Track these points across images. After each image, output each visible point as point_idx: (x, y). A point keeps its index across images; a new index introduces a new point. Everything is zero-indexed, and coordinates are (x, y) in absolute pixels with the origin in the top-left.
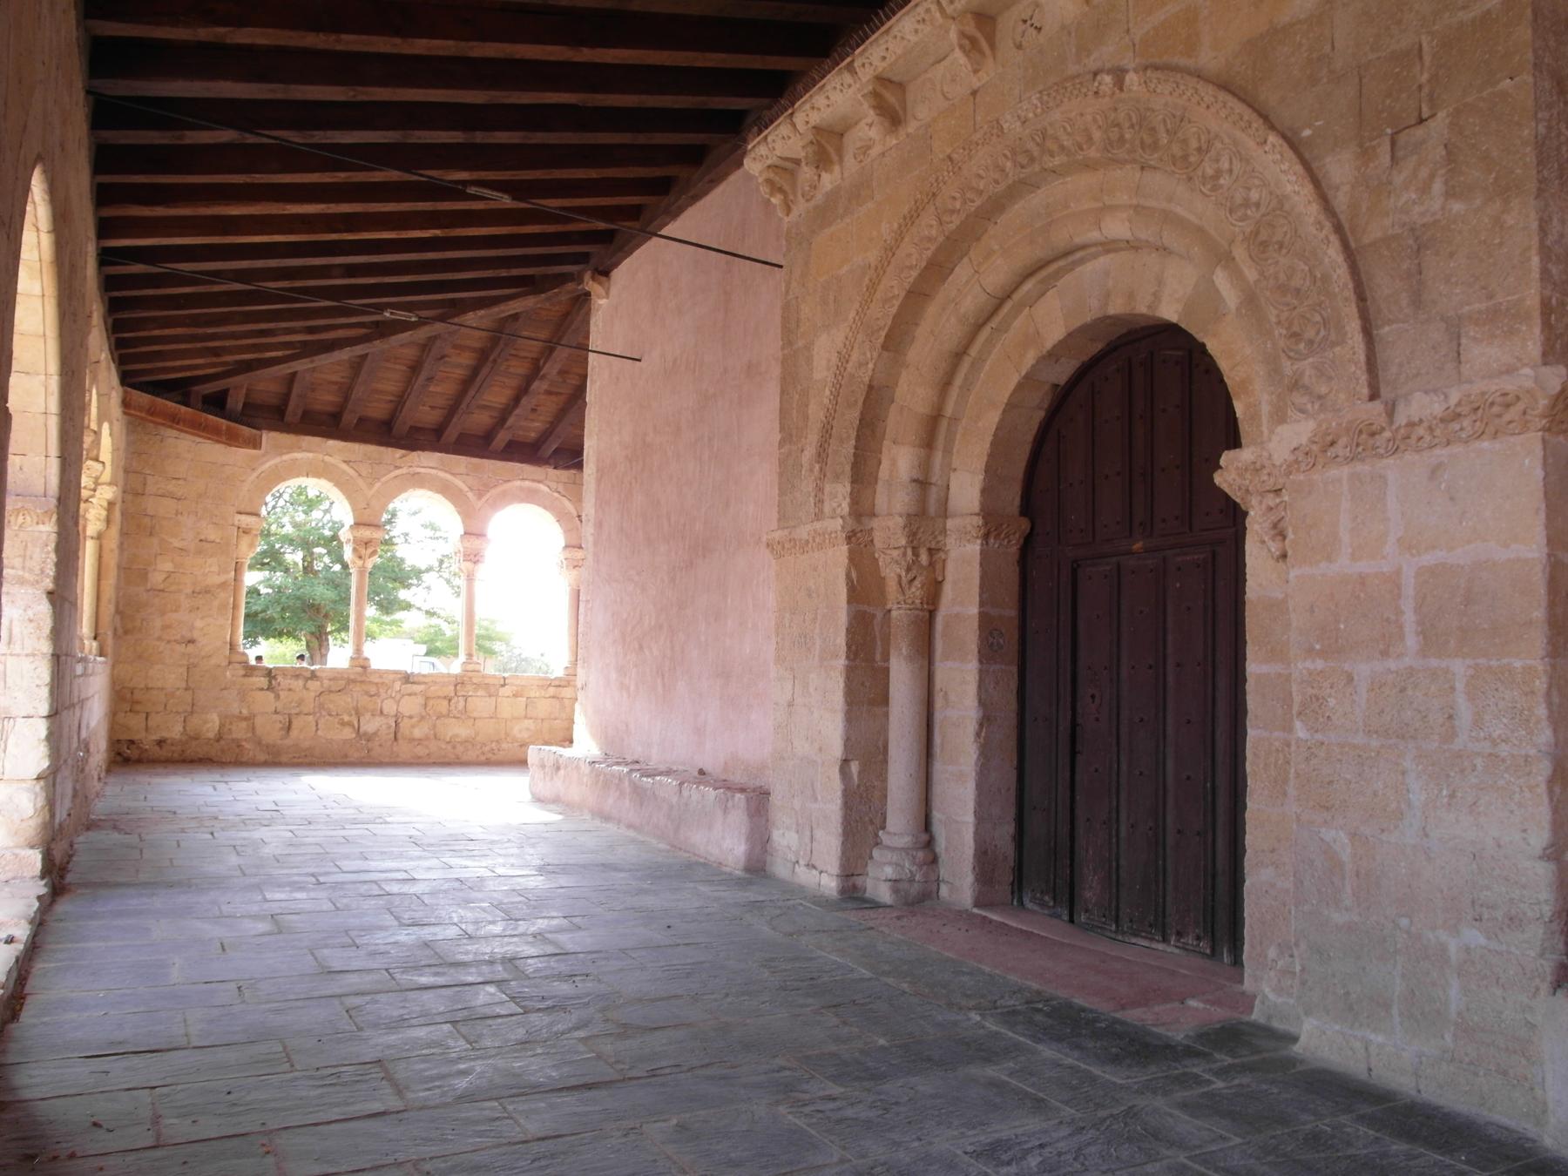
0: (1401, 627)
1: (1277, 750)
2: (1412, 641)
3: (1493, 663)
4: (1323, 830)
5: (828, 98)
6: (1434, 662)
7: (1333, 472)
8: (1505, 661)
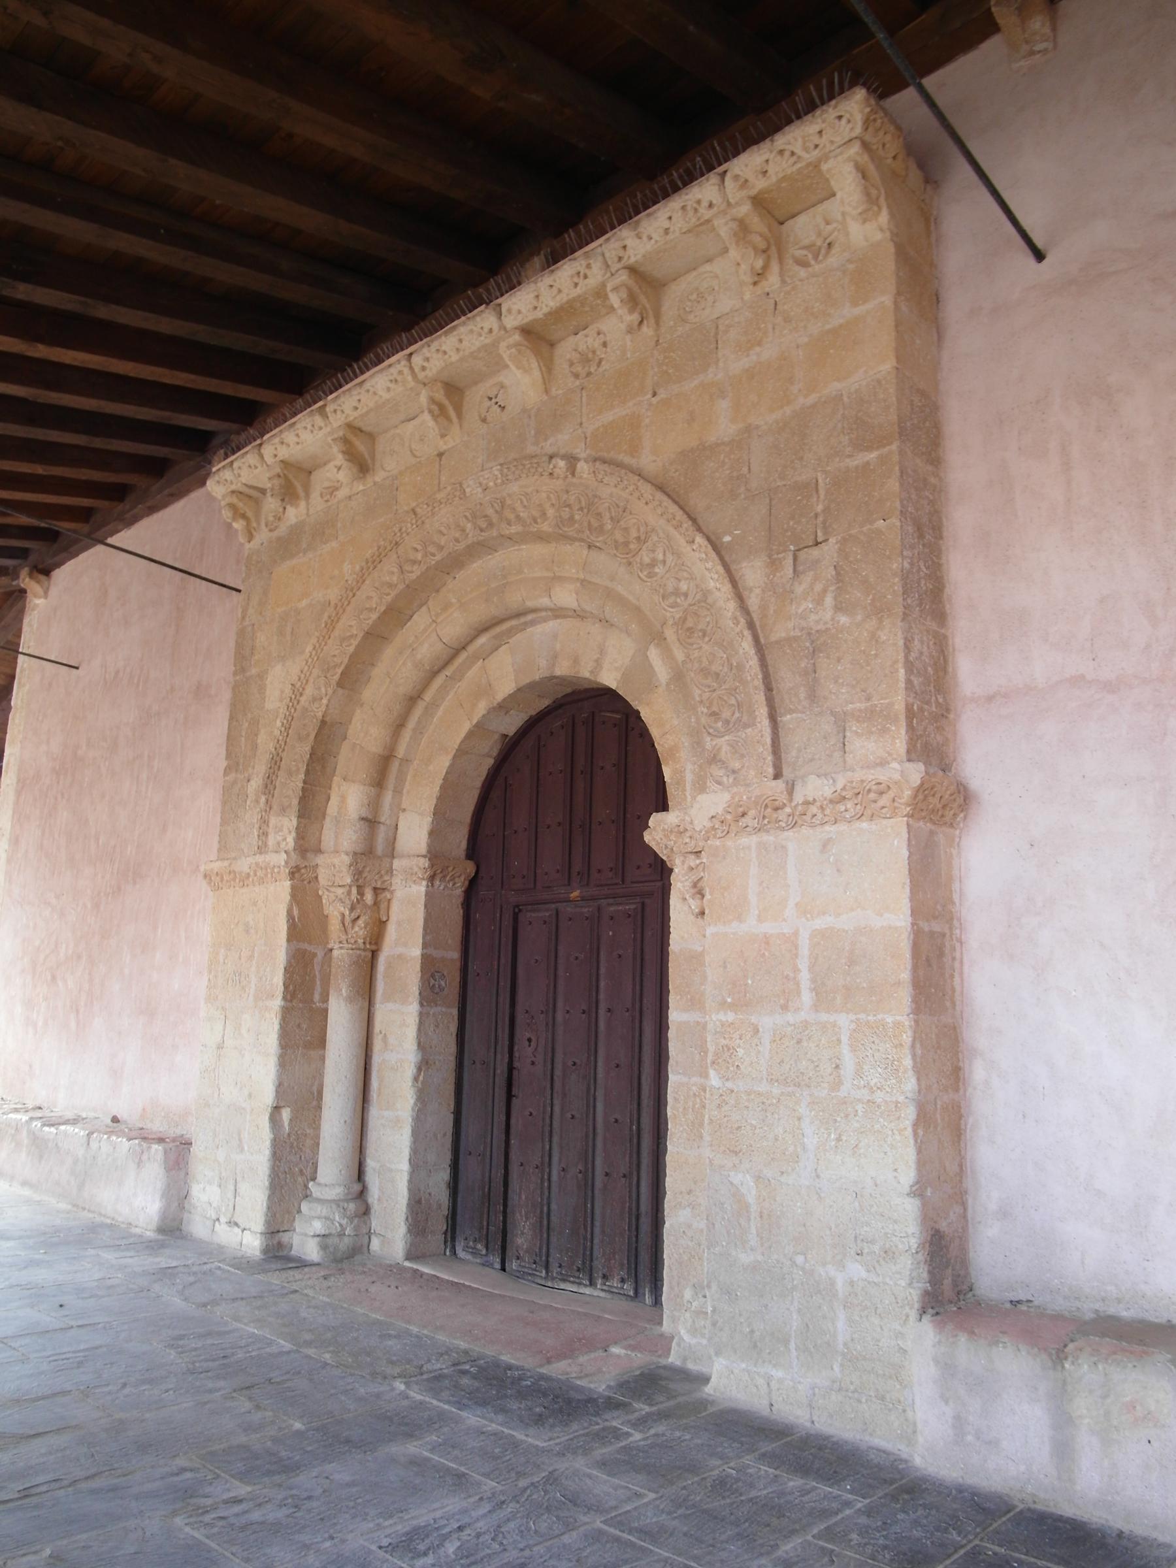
0: (798, 984)
1: (695, 1094)
2: (807, 997)
3: (869, 1018)
4: (732, 1174)
5: (297, 435)
6: (824, 1017)
7: (744, 840)
8: (880, 1017)
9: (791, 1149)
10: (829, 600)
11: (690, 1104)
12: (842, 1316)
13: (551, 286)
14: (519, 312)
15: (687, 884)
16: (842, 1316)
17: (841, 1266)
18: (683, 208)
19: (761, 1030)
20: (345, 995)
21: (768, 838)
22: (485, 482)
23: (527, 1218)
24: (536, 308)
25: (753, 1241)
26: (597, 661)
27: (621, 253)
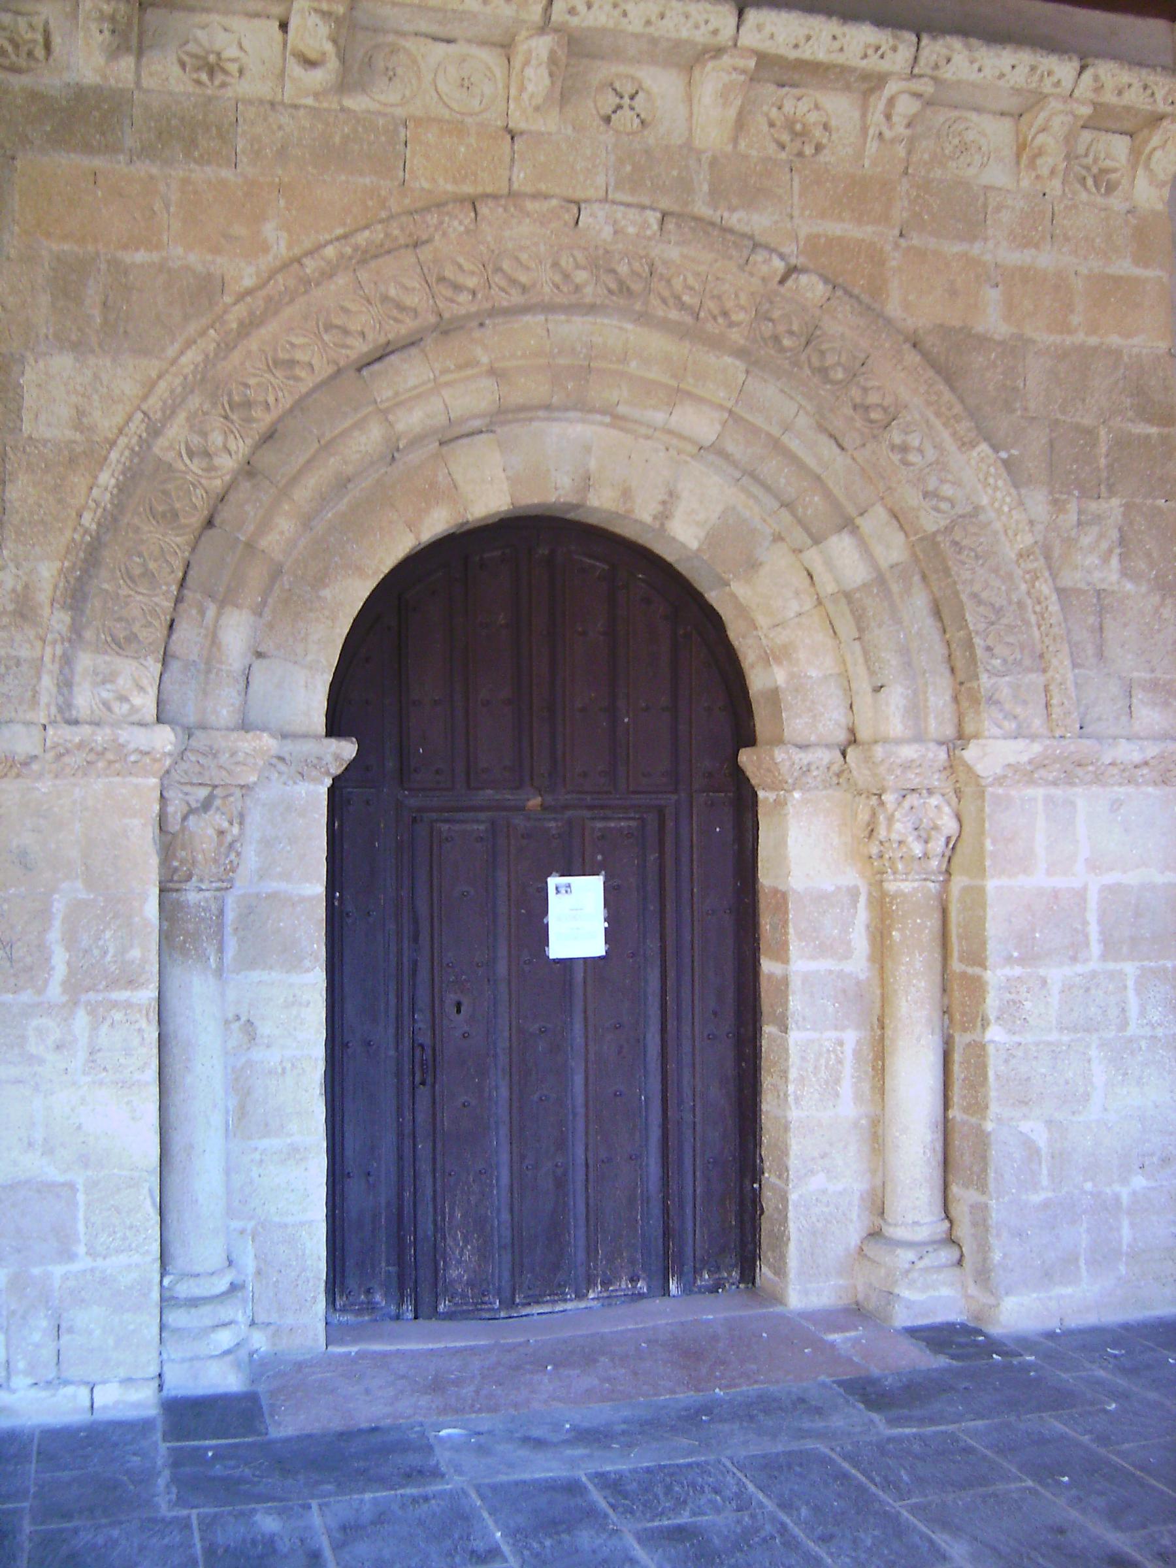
0: (1086, 936)
1: (828, 1050)
2: (1096, 948)
6: (1111, 966)
7: (1030, 792)
9: (1081, 1090)
10: (1114, 562)
11: (823, 1061)
12: (1125, 1223)
13: (834, 38)
14: (772, 36)
15: (910, 825)
16: (1125, 1223)
17: (1125, 1181)
18: (1033, 69)
19: (1049, 981)
20: (214, 966)
21: (1057, 792)
22: (623, 223)
23: (466, 1242)
24: (796, 46)
25: (1045, 1181)
26: (664, 503)
27: (943, 62)
